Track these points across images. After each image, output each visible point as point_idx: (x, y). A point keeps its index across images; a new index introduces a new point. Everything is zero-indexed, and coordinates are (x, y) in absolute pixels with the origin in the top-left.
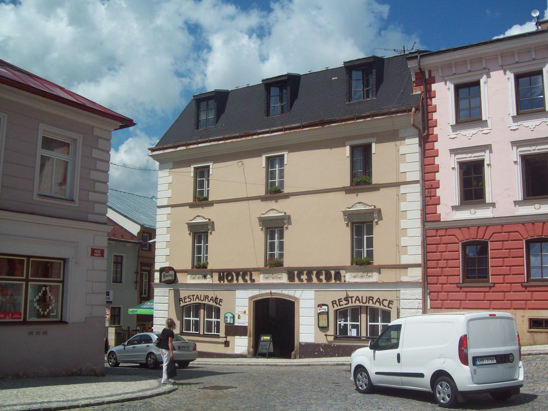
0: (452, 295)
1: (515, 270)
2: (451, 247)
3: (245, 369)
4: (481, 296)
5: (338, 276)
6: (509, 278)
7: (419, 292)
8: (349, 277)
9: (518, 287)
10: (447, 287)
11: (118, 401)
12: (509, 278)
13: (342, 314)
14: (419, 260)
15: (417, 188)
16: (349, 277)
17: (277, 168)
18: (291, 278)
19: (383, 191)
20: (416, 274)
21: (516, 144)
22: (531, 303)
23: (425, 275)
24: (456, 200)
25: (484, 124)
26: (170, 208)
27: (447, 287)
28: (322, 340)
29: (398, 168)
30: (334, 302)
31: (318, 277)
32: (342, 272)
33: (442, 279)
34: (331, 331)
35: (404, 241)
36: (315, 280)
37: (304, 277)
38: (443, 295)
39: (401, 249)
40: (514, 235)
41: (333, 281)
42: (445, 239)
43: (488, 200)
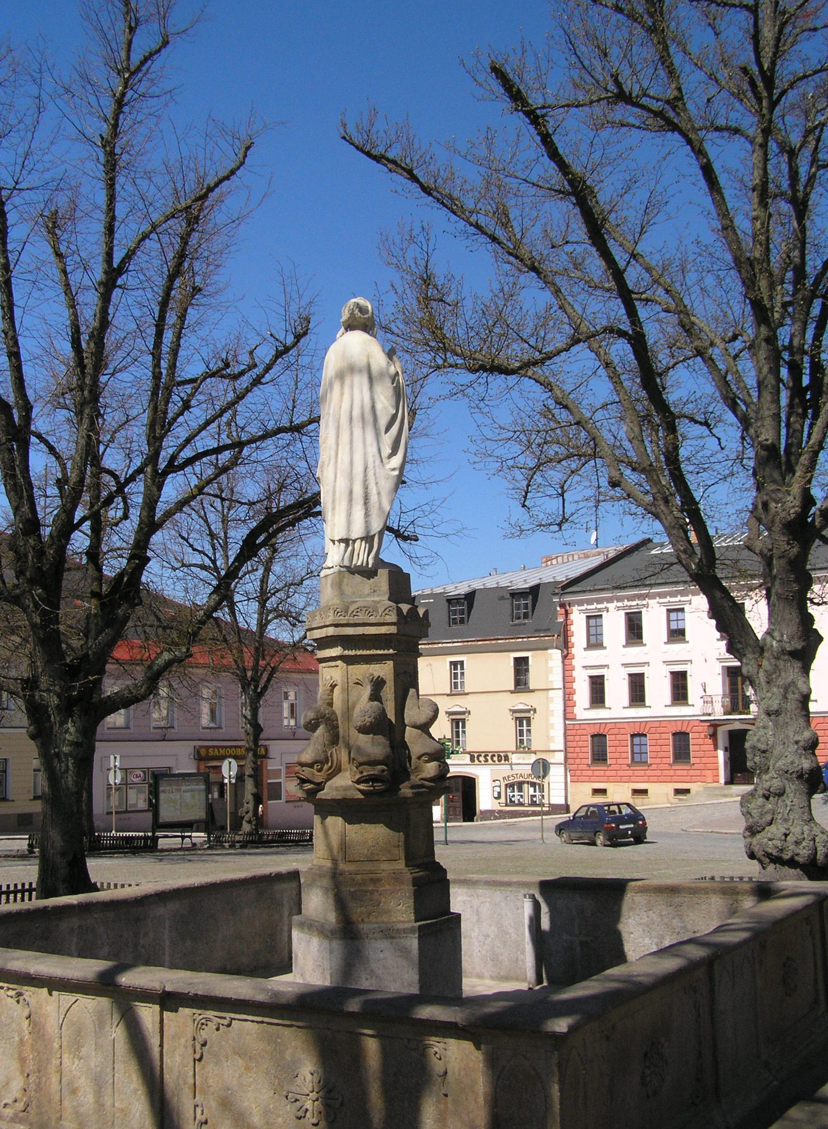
0: (585, 773)
1: (624, 755)
2: (584, 738)
3: (523, 824)
4: (685, 773)
5: (507, 758)
6: (620, 761)
7: (562, 768)
8: (514, 758)
9: (625, 767)
10: (581, 767)
11: (501, 842)
12: (620, 761)
13: (511, 786)
14: (562, 747)
15: (561, 693)
16: (514, 758)
17: (459, 671)
18: (472, 759)
19: (536, 694)
20: (560, 757)
21: (625, 665)
22: (633, 779)
23: (566, 758)
24: (587, 704)
25: (605, 648)
26: (552, 748)
27: (581, 767)
28: (497, 807)
29: (547, 678)
30: (504, 778)
31: (492, 759)
32: (509, 755)
33: (578, 761)
34: (503, 800)
35: (552, 733)
36: (490, 761)
37: (482, 759)
38: (578, 773)
39: (549, 738)
40: (622, 731)
41: (503, 762)
42: (579, 732)
43: (607, 705)
